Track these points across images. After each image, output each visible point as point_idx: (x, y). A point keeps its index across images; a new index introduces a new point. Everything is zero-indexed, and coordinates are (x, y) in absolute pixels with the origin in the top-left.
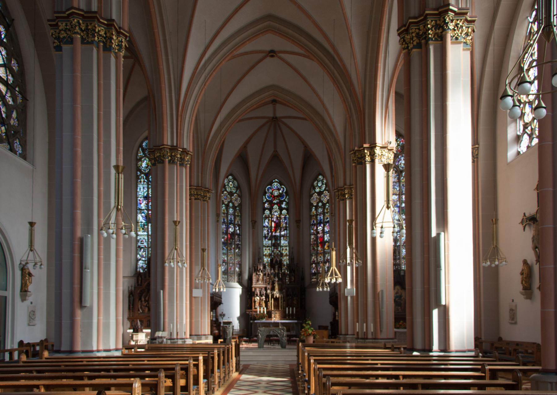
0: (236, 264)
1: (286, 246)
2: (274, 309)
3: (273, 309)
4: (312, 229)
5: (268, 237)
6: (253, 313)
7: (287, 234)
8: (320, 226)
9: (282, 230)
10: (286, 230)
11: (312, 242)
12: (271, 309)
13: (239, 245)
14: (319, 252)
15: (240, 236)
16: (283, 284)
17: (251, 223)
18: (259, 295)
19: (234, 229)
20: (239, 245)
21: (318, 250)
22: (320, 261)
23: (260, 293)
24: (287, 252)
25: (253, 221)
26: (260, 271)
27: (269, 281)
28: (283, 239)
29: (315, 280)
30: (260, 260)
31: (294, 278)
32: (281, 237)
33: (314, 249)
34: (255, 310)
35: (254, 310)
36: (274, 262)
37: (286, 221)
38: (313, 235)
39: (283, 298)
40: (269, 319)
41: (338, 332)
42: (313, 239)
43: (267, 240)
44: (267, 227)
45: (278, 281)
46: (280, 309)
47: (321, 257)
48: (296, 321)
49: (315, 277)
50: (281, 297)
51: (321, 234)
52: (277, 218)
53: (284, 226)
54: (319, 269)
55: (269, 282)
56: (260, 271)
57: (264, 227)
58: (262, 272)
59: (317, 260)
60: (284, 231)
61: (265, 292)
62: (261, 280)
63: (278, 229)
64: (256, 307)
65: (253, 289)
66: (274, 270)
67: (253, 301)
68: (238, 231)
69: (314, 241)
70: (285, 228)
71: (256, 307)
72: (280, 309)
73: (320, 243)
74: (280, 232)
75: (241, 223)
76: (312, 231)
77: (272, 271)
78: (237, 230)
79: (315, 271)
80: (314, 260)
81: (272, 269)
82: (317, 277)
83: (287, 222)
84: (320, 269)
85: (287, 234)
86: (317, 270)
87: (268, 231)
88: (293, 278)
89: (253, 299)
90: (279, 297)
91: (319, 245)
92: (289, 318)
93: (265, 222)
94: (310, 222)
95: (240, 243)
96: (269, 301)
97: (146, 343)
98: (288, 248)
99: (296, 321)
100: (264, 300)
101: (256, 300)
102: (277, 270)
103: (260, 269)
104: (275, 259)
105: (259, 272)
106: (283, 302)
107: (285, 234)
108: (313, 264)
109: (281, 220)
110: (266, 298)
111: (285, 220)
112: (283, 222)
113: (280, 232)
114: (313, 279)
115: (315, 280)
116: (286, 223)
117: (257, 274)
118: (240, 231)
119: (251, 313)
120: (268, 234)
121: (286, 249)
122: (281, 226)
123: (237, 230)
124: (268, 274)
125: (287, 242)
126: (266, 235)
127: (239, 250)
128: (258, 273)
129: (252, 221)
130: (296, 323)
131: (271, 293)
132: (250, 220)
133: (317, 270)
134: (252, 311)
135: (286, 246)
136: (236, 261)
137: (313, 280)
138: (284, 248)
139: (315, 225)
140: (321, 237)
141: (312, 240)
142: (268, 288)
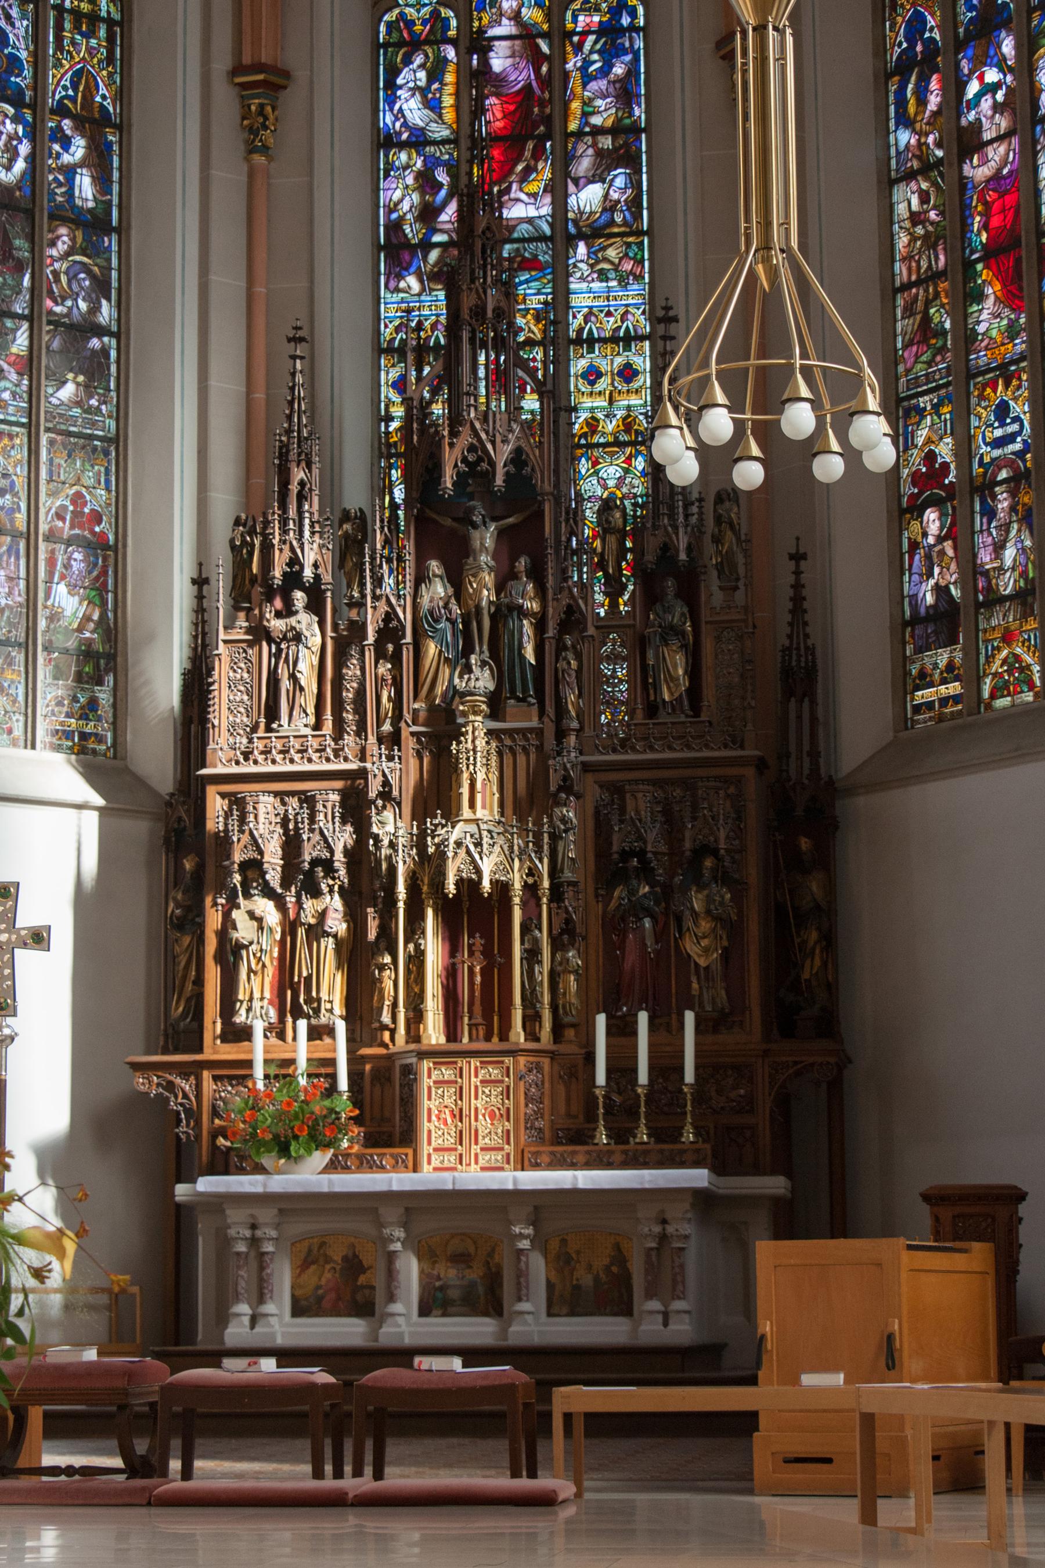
0: (51, 537)
1: (627, 340)
2: (452, 1033)
3: (434, 1033)
4: (905, 121)
5: (426, 245)
6: (208, 1085)
7: (635, 203)
8: (987, 57)
9: (584, 165)
10: (626, 158)
11: (907, 258)
12: (414, 1036)
13: (100, 331)
14: (981, 358)
15: (112, 242)
16: (561, 734)
17: (224, 96)
18: (273, 877)
19: (32, 159)
20: (100, 331)
21: (968, 338)
22: (997, 463)
23: (292, 845)
24: (635, 401)
25: (258, 67)
26: (299, 597)
27: (397, 701)
28: (595, 258)
29: (954, 688)
30: (298, 474)
31: (694, 672)
32: (571, 241)
33: (927, 331)
34: (228, 1052)
35: (215, 1050)
36: (448, 481)
37: (619, 70)
38: (910, 176)
39: (556, 894)
40: (386, 1155)
41: (636, 1079)
42: (916, 218)
43: (412, 282)
44: (418, 140)
45: (496, 705)
46: (518, 1034)
47: (1002, 411)
48: (698, 1177)
49: (943, 657)
50: (531, 889)
51: (996, 153)
52: (527, 35)
53: (596, 120)
54: (985, 557)
55: (397, 717)
56: (299, 597)
57: (388, 142)
58: (315, 606)
59: (965, 449)
60: (597, 177)
61: (343, 838)
62: (308, 700)
63: (538, 153)
64: (241, 1018)
65: (216, 805)
66: (456, 579)
67: (211, 945)
68: (85, 186)
69: (930, 242)
70: (606, 142)
71: (241, 1018)
72: (518, 1034)
73: (990, 254)
74: (558, 191)
75: (122, 95)
76: (904, 137)
77: (438, 590)
78: (70, 171)
79: (941, 591)
80: (930, 457)
81: (435, 566)
82: (972, 653)
83: (632, 72)
84: (999, 548)
85: (635, 203)
86: (971, 570)
87: (426, 182)
88: (678, 665)
89: (213, 920)
90: (502, 888)
91: (985, 274)
92: (619, 1135)
93: (391, 86)
94: (880, 49)
95: (106, 313)
96: (387, 940)
97: (138, 1453)
98: (642, 360)
99: (698, 1177)
100: (337, 924)
101: (244, 930)
102: (489, 579)
103: (293, 579)
104: (465, 439)
105: (288, 611)
106: (556, 945)
107: (609, 206)
108: (917, 510)
109: (572, 63)
110: (354, 916)
111: (610, 54)
112: (587, 78)
113: (558, 191)
114: (924, 680)
115: (954, 688)
116: (625, 94)
117: (259, 633)
118: (102, 181)
119: (186, 1086)
120: (428, 214)
121: (628, 373)
122: (573, 126)
123: (70, 171)
124: (389, 631)
125: (634, 295)
126: (412, 231)
127: (88, 388)
128: (277, 625)
129: (238, 69)
130: (702, 1199)
131: (420, 844)
132: (222, 64)
133: (971, 570)
134: (192, 1070)
135: (627, 340)
136: (48, 505)
137: (924, 695)
138: (610, 361)
139: (928, 64)
140: (996, 177)
141: (902, 241)
142: (374, 788)
